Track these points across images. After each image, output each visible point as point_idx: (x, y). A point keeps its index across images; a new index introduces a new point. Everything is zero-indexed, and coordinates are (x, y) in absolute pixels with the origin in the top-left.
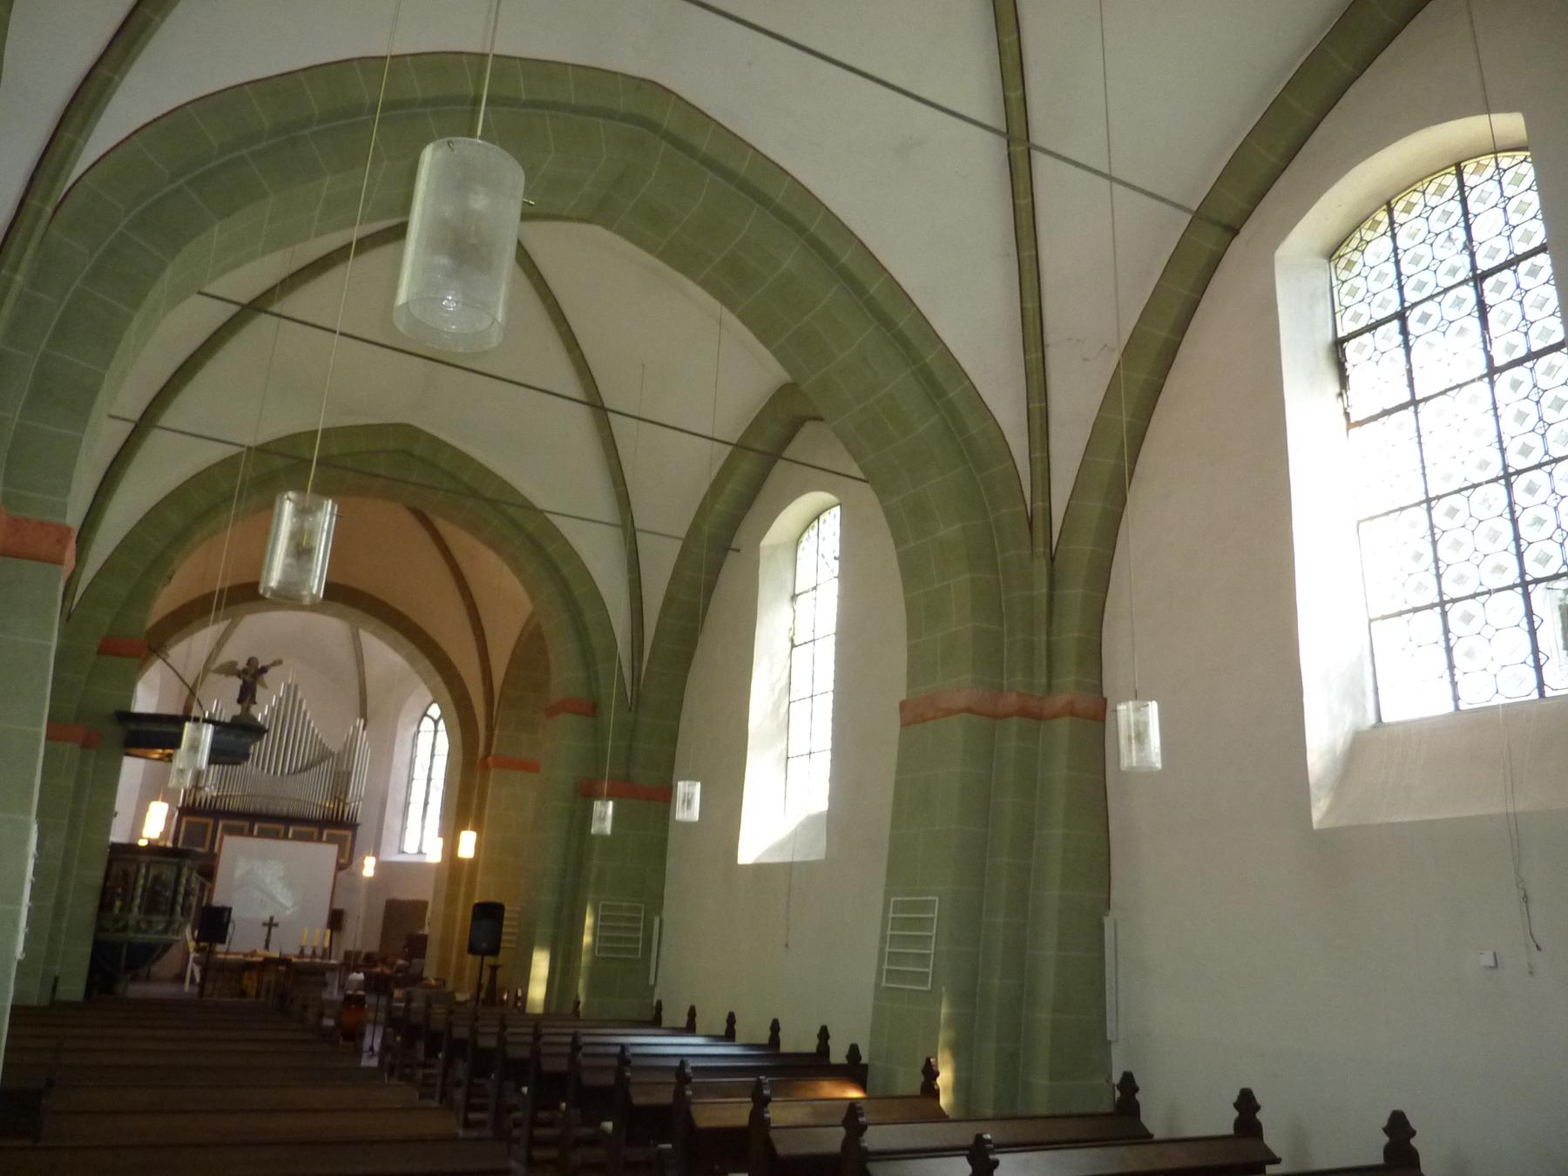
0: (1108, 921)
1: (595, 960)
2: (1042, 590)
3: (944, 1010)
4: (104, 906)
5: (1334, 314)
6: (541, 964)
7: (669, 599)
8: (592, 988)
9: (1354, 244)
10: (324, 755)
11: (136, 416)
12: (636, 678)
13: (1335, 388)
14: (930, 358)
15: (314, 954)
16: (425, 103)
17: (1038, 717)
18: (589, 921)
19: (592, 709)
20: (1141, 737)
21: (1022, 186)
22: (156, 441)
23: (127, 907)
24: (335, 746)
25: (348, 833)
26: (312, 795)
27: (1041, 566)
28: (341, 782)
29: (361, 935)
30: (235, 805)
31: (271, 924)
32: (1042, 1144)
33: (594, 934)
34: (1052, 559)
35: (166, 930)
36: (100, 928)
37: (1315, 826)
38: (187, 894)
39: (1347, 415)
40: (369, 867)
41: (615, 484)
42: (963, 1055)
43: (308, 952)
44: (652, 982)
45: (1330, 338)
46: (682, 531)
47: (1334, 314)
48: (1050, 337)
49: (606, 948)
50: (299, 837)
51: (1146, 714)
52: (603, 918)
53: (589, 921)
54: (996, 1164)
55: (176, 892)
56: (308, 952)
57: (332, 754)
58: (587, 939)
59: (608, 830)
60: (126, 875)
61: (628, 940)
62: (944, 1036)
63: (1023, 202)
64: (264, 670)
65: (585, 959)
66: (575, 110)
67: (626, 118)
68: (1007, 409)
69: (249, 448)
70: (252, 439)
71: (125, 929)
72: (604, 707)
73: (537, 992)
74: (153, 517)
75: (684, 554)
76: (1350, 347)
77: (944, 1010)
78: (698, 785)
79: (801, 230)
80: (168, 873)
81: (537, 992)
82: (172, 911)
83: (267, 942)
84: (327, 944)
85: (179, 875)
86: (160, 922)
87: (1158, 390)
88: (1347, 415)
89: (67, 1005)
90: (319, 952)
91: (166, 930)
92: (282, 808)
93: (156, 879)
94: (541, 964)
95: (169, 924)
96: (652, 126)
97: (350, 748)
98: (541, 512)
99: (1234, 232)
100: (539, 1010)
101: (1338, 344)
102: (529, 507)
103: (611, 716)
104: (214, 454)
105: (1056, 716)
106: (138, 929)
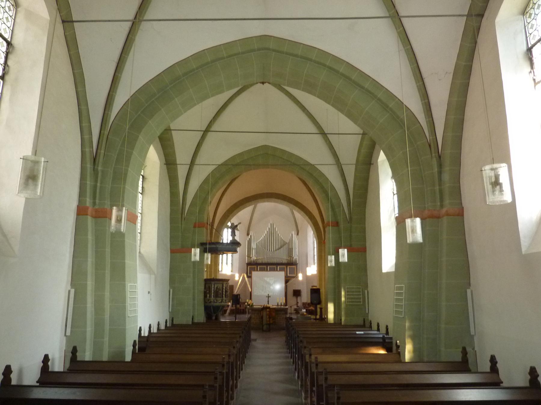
0: (469, 291)
1: (346, 305)
2: (436, 170)
3: (407, 324)
4: (205, 296)
5: (527, 37)
6: (331, 307)
7: (355, 184)
8: (347, 315)
9: (531, 7)
10: (285, 243)
11: (189, 163)
12: (350, 213)
13: (529, 69)
14: (380, 95)
15: (281, 305)
16: (197, 68)
17: (438, 217)
18: (343, 293)
19: (336, 224)
20: (413, 231)
21: (86, 131)
22: (196, 168)
23: (210, 296)
24: (287, 241)
25: (295, 267)
26: (282, 256)
27: (435, 162)
28: (290, 251)
29: (305, 297)
30: (260, 261)
31: (268, 297)
32: (436, 371)
33: (345, 297)
34: (440, 157)
35: (222, 302)
36: (205, 302)
37: (523, 253)
38: (226, 292)
39: (534, 80)
40: (300, 277)
41: (330, 150)
42: (415, 339)
43: (280, 304)
44: (367, 312)
45: (525, 48)
46: (354, 162)
47: (527, 37)
48: (424, 76)
49: (350, 302)
50: (271, 270)
51: (415, 222)
52: (348, 292)
53: (343, 293)
54: (37, 382)
55: (223, 291)
56: (280, 304)
57: (287, 243)
58: (343, 299)
59: (334, 265)
60: (209, 287)
61: (357, 298)
62: (408, 333)
63: (86, 137)
64: (237, 226)
65: (343, 306)
66: (243, 53)
67: (259, 49)
68: (413, 104)
69: (219, 165)
70: (220, 162)
71: (211, 302)
72: (346, 224)
73: (331, 316)
74: (201, 187)
75: (356, 169)
76: (534, 50)
77: (407, 324)
78: (346, 250)
79: (325, 65)
80: (220, 286)
81: (331, 316)
82: (222, 297)
83: (268, 302)
84: (284, 302)
85: (223, 286)
86: (219, 300)
87: (468, 85)
88: (534, 80)
89: (198, 324)
90: (283, 304)
91: (222, 302)
92: (275, 261)
93: (217, 288)
94: (331, 307)
95: (222, 300)
96: (268, 49)
97: (291, 240)
98: (313, 165)
99: (482, 16)
100: (147, 334)
101: (529, 50)
102: (309, 164)
103: (342, 226)
104: (211, 168)
105: (443, 216)
106: (214, 302)
